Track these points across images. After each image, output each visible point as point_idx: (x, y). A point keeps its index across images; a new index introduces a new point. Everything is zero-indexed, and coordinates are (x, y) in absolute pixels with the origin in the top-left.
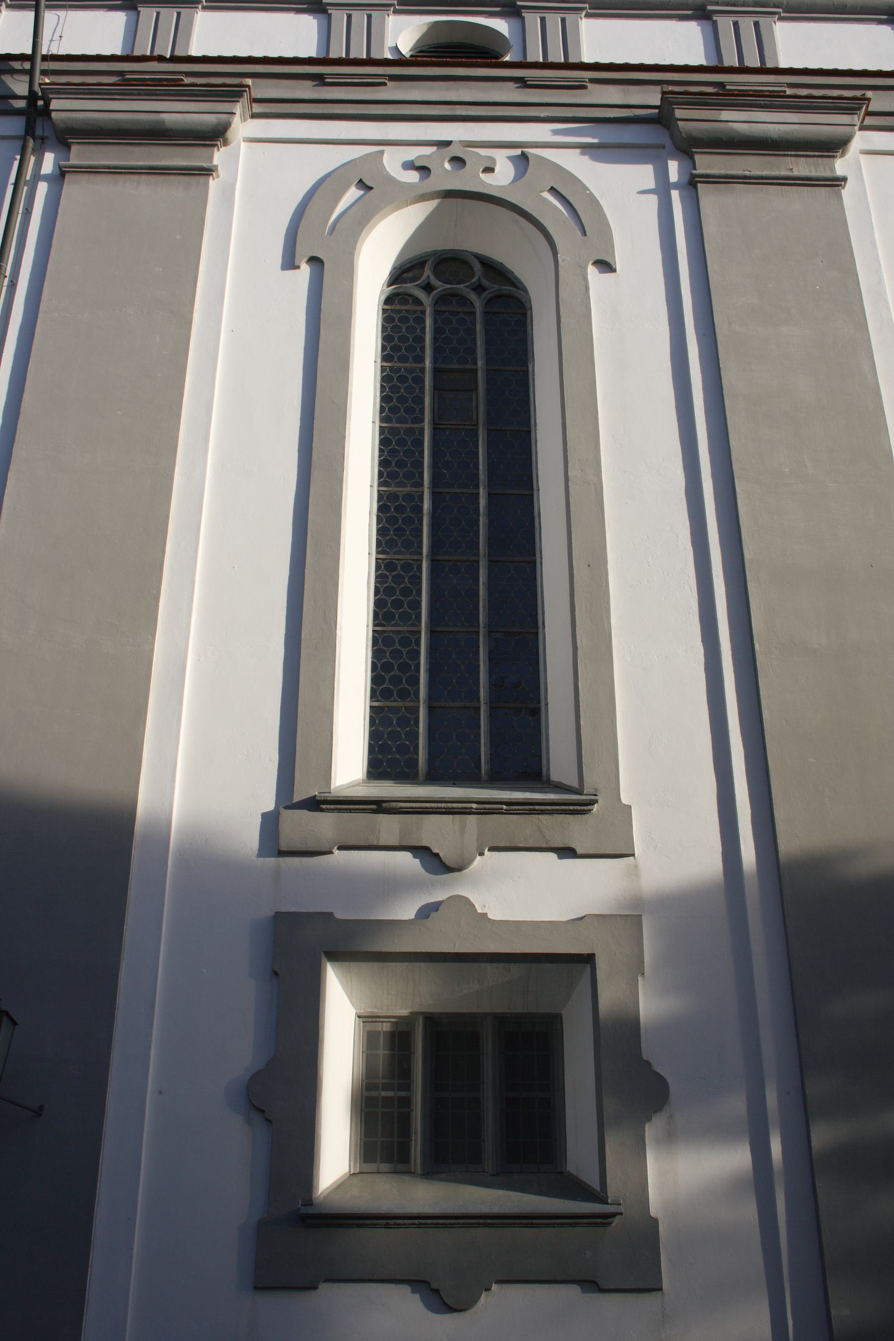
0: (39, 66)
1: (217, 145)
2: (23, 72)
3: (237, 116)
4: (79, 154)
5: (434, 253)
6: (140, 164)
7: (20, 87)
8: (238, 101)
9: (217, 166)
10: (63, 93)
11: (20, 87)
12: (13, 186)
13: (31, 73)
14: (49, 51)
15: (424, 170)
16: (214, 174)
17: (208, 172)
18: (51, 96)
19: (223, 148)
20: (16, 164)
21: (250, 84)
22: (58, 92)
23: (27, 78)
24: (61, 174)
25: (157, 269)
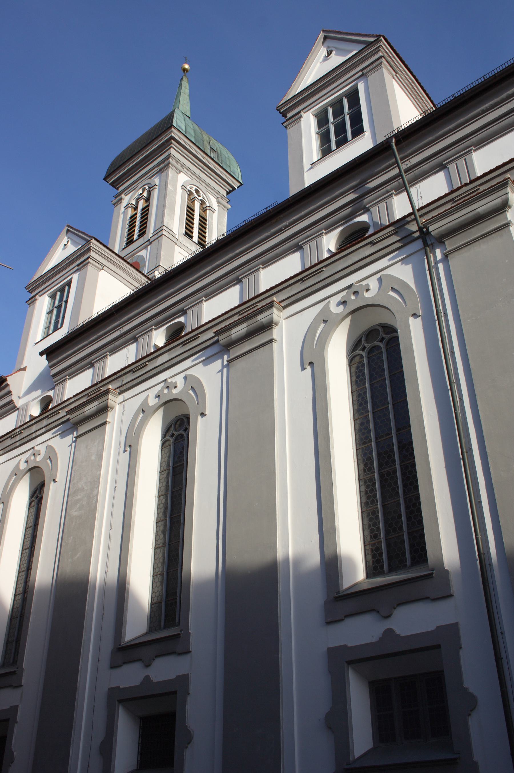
0: (418, 214)
1: (506, 210)
2: (412, 220)
3: (509, 193)
4: (450, 244)
5: (363, 334)
6: (477, 236)
7: (413, 227)
8: (507, 187)
9: (510, 220)
10: (432, 222)
11: (413, 227)
12: (428, 271)
13: (416, 219)
14: (419, 206)
15: (344, 303)
16: (511, 224)
17: (507, 225)
18: (428, 226)
19: (510, 210)
20: (426, 260)
21: (509, 176)
22: (430, 223)
23: (415, 222)
24: (446, 256)
25: (503, 280)
